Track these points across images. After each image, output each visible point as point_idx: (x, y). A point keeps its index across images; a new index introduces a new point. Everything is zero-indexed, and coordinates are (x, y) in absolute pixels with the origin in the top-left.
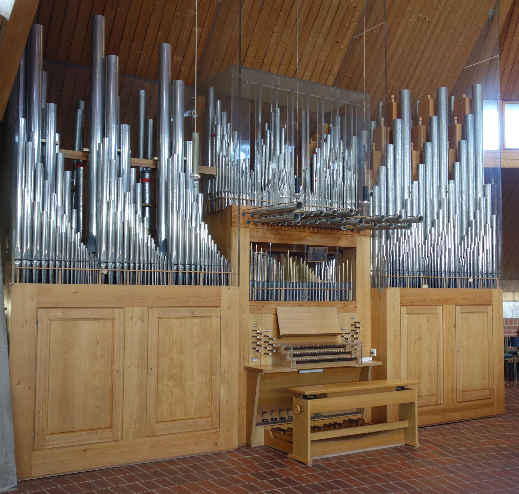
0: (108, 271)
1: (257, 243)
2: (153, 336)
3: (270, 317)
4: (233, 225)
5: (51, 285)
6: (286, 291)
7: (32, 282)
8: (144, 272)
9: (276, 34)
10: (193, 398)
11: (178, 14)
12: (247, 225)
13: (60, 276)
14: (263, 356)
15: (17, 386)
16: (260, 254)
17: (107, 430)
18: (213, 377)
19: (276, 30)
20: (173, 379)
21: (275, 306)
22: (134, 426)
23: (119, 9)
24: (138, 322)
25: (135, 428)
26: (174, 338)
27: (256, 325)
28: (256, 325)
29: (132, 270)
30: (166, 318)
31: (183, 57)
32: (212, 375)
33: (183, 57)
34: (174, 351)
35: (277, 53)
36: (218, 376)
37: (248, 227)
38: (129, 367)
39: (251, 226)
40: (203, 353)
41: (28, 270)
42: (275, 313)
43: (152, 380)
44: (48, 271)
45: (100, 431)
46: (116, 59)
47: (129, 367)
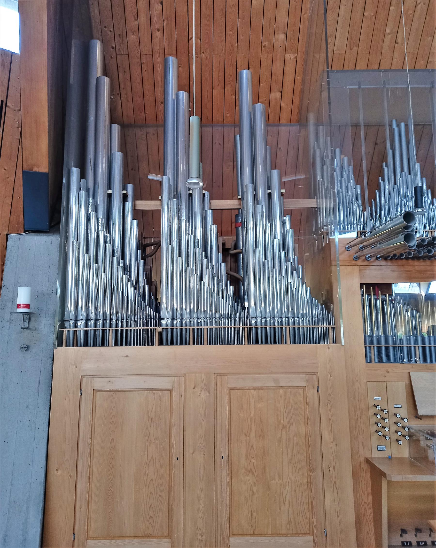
0: (163, 329)
1: (374, 285)
2: (223, 412)
3: (401, 388)
4: (333, 263)
5: (124, 347)
6: (424, 349)
7: (96, 346)
8: (117, 331)
9: (390, 36)
10: (284, 503)
11: (266, 43)
12: (354, 262)
13: (288, 334)
14: (394, 444)
15: (56, 472)
16: (379, 299)
17: (165, 540)
18: (313, 474)
19: (388, 31)
20: (253, 473)
21: (408, 371)
22: (200, 537)
23: (203, 55)
24: (203, 392)
25: (202, 541)
26: (252, 415)
27: (380, 399)
28: (380, 399)
29: (291, 325)
30: (240, 388)
31: (281, 92)
32: (310, 471)
33: (281, 92)
34: (253, 434)
35: (395, 60)
36: (320, 473)
37: (356, 265)
38: (193, 453)
39: (359, 262)
40: (295, 438)
41: (272, 328)
42: (407, 381)
43: (224, 473)
44: (256, 329)
45: (155, 540)
46: (183, 94)
47: (193, 453)
